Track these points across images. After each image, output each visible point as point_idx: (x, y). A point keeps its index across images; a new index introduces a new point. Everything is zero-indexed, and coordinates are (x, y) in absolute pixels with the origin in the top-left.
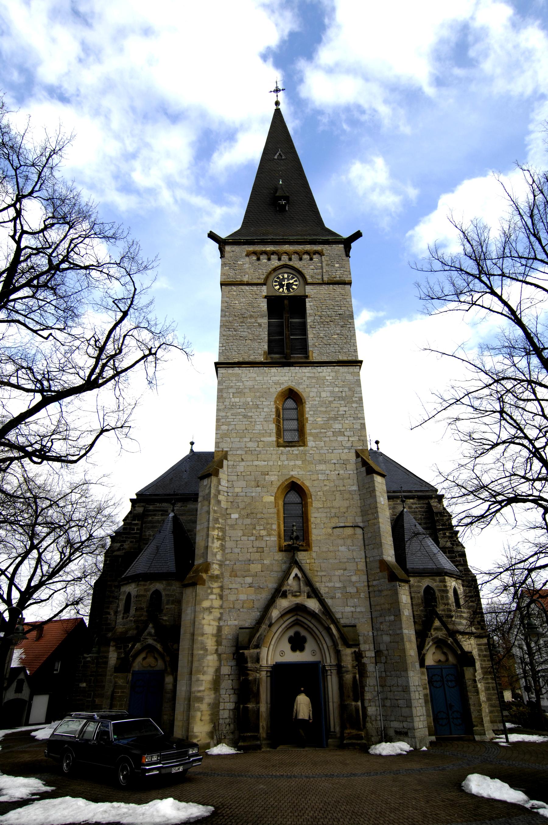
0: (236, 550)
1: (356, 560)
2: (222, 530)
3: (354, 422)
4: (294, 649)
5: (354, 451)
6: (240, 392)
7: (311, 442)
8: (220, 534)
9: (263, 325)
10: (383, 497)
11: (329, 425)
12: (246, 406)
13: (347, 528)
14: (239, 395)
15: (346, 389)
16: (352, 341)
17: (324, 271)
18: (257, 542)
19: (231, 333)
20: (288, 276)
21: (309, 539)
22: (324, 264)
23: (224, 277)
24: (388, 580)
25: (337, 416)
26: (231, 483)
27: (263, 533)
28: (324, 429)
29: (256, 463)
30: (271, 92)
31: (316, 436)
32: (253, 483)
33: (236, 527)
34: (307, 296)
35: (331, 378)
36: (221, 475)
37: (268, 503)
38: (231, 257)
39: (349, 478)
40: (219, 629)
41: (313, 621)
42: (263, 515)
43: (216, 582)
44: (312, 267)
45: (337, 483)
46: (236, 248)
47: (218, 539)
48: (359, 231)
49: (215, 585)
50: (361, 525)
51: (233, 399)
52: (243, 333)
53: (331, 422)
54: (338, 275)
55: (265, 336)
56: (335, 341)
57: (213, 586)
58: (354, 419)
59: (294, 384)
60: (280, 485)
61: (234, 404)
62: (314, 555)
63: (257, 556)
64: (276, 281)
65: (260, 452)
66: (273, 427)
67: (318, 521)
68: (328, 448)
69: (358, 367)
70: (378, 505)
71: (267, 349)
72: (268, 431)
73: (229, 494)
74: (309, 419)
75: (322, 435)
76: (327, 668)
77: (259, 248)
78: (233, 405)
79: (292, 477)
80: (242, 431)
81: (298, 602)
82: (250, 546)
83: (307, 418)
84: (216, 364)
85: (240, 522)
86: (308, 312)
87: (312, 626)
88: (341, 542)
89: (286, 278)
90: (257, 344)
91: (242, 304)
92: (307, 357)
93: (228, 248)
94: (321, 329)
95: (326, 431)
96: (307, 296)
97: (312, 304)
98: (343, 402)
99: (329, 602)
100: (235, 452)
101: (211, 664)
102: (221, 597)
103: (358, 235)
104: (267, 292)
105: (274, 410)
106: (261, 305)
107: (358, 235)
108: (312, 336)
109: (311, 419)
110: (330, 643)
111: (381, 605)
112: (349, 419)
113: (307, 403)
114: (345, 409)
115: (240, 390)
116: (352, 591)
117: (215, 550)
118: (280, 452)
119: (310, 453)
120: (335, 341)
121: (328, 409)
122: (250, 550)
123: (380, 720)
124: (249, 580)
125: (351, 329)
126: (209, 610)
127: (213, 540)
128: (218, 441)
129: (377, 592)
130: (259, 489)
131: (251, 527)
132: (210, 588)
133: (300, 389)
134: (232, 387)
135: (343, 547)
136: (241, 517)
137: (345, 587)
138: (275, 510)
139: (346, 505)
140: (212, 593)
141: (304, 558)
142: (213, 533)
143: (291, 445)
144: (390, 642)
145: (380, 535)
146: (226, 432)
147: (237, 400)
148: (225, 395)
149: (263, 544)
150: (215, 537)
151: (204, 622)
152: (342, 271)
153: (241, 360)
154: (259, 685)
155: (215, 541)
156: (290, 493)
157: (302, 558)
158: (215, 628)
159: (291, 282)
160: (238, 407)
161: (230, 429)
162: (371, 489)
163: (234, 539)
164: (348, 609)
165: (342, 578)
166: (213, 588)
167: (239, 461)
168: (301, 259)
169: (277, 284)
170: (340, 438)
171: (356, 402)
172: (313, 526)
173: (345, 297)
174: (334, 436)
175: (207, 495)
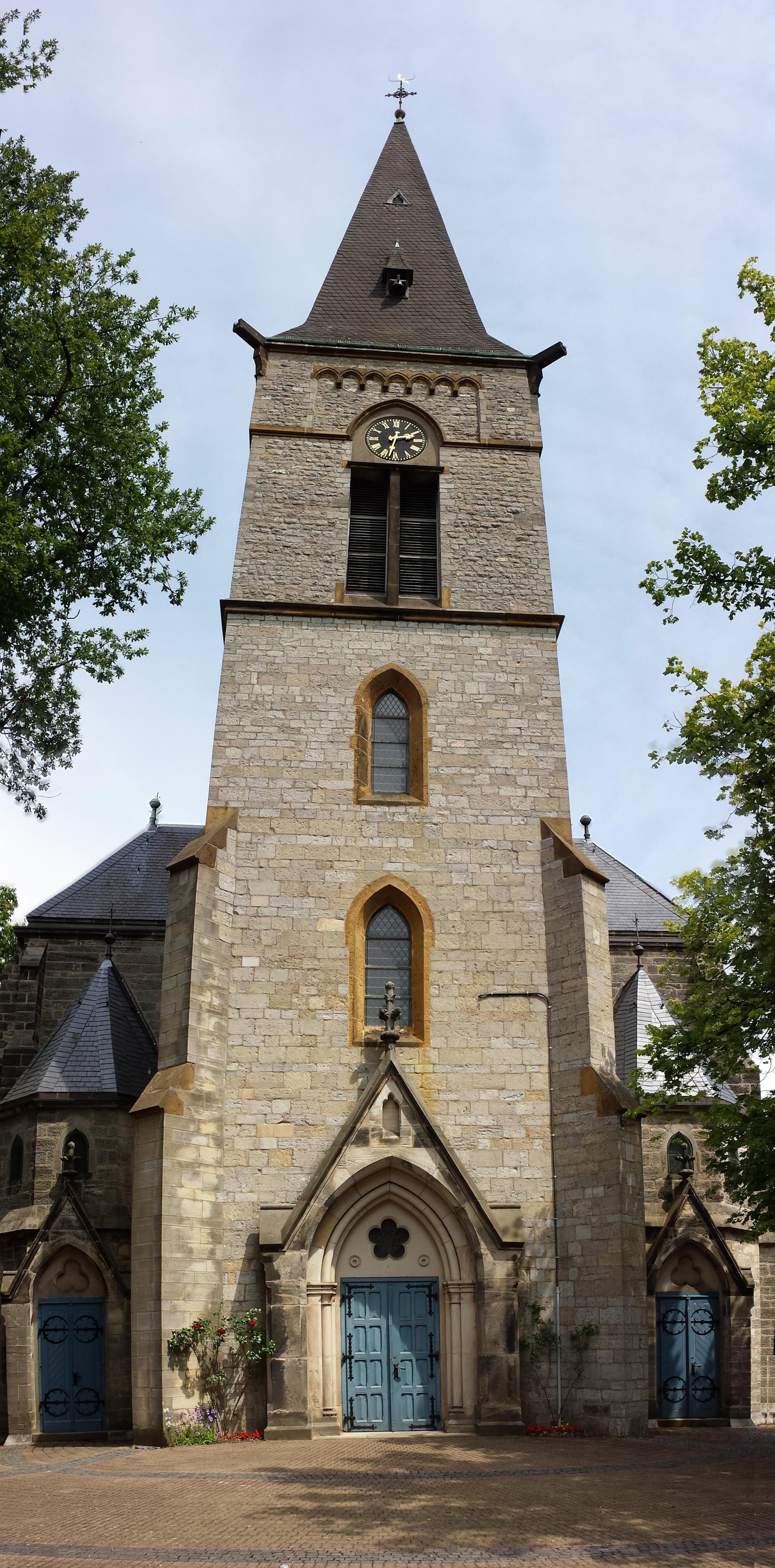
0: (254, 1040)
1: (529, 1069)
2: (222, 993)
3: (541, 754)
4: (380, 1253)
5: (537, 822)
6: (274, 672)
7: (436, 795)
8: (216, 1002)
9: (338, 525)
10: (599, 928)
11: (482, 757)
12: (287, 705)
13: (512, 998)
14: (271, 678)
15: (524, 679)
16: (540, 572)
17: (483, 419)
18: (302, 1022)
19: (262, 536)
20: (402, 426)
21: (422, 1022)
22: (483, 406)
23: (259, 416)
24: (599, 1111)
25: (501, 739)
26: (242, 883)
27: (316, 1002)
28: (470, 767)
29: (305, 840)
30: (389, 95)
31: (448, 783)
32: (296, 886)
33: (254, 987)
34: (441, 470)
35: (490, 650)
36: (220, 865)
37: (330, 933)
38: (279, 377)
39: (523, 884)
40: (217, 1209)
41: (424, 1196)
42: (316, 962)
43: (208, 1108)
44: (456, 410)
45: (493, 892)
46: (294, 364)
47: (212, 1012)
48: (560, 343)
49: (205, 1114)
50: (545, 991)
51: (257, 686)
52: (292, 539)
53: (486, 751)
54: (512, 430)
55: (340, 548)
56: (501, 569)
57: (200, 1118)
58: (540, 749)
59: (403, 659)
60: (360, 894)
61: (261, 699)
62: (433, 1055)
63: (301, 1054)
64: (374, 434)
65: (315, 813)
66: (348, 756)
67: (445, 979)
68: (477, 813)
69: (553, 631)
70: (588, 946)
71: (345, 578)
72: (337, 766)
73: (238, 910)
74: (434, 742)
75: (464, 781)
76: (452, 1290)
77: (340, 365)
78: (257, 702)
79: (389, 875)
80: (274, 763)
81: (394, 1154)
82: (286, 1031)
83: (431, 739)
84: (224, 604)
85: (261, 975)
86: (442, 502)
87: (422, 1206)
88: (497, 1028)
89: (397, 429)
90: (322, 565)
91: (295, 477)
92: (438, 603)
93: (274, 363)
94: (471, 541)
95: (473, 771)
96: (441, 470)
97: (452, 486)
98: (515, 708)
99: (462, 1157)
100: (255, 813)
101: (200, 1280)
102: (219, 1142)
103: (557, 352)
104: (353, 455)
105: (353, 717)
106: (338, 480)
107: (557, 352)
108: (450, 555)
109: (438, 742)
110: (459, 1240)
111: (577, 1164)
112: (527, 746)
113: (432, 705)
114: (520, 723)
115: (275, 667)
116: (515, 1135)
117: (205, 1038)
118: (362, 816)
119: (435, 821)
120: (501, 569)
121: (481, 722)
122: (286, 1041)
123: (557, 1386)
124: (282, 1106)
125: (538, 545)
126: (194, 1168)
127: (199, 1014)
128: (217, 783)
129: (571, 1138)
130: (309, 902)
131: (289, 988)
132: (193, 1120)
133: (416, 672)
134: (256, 659)
135: (501, 1039)
136: (266, 963)
137: (499, 1127)
138: (346, 952)
139: (513, 946)
140: (198, 1132)
141: (410, 1062)
142: (201, 998)
143: (389, 799)
144: (592, 1240)
145: (586, 1015)
146: (236, 763)
147: (267, 689)
148: (239, 677)
149: (316, 1029)
150: (205, 1007)
151: (181, 1192)
152: (521, 423)
153: (282, 598)
154: (304, 1322)
155: (205, 1016)
156: (381, 915)
157: (405, 1062)
158: (208, 1207)
159: (408, 436)
160: (268, 707)
161: (247, 756)
162: (575, 909)
163: (248, 1013)
164: (506, 1172)
165: (495, 1108)
166: (199, 1121)
167: (264, 834)
168: (432, 393)
169: (377, 439)
170: (506, 791)
171: (546, 708)
172: (433, 991)
173: (527, 476)
174: (491, 784)
175: (186, 908)
